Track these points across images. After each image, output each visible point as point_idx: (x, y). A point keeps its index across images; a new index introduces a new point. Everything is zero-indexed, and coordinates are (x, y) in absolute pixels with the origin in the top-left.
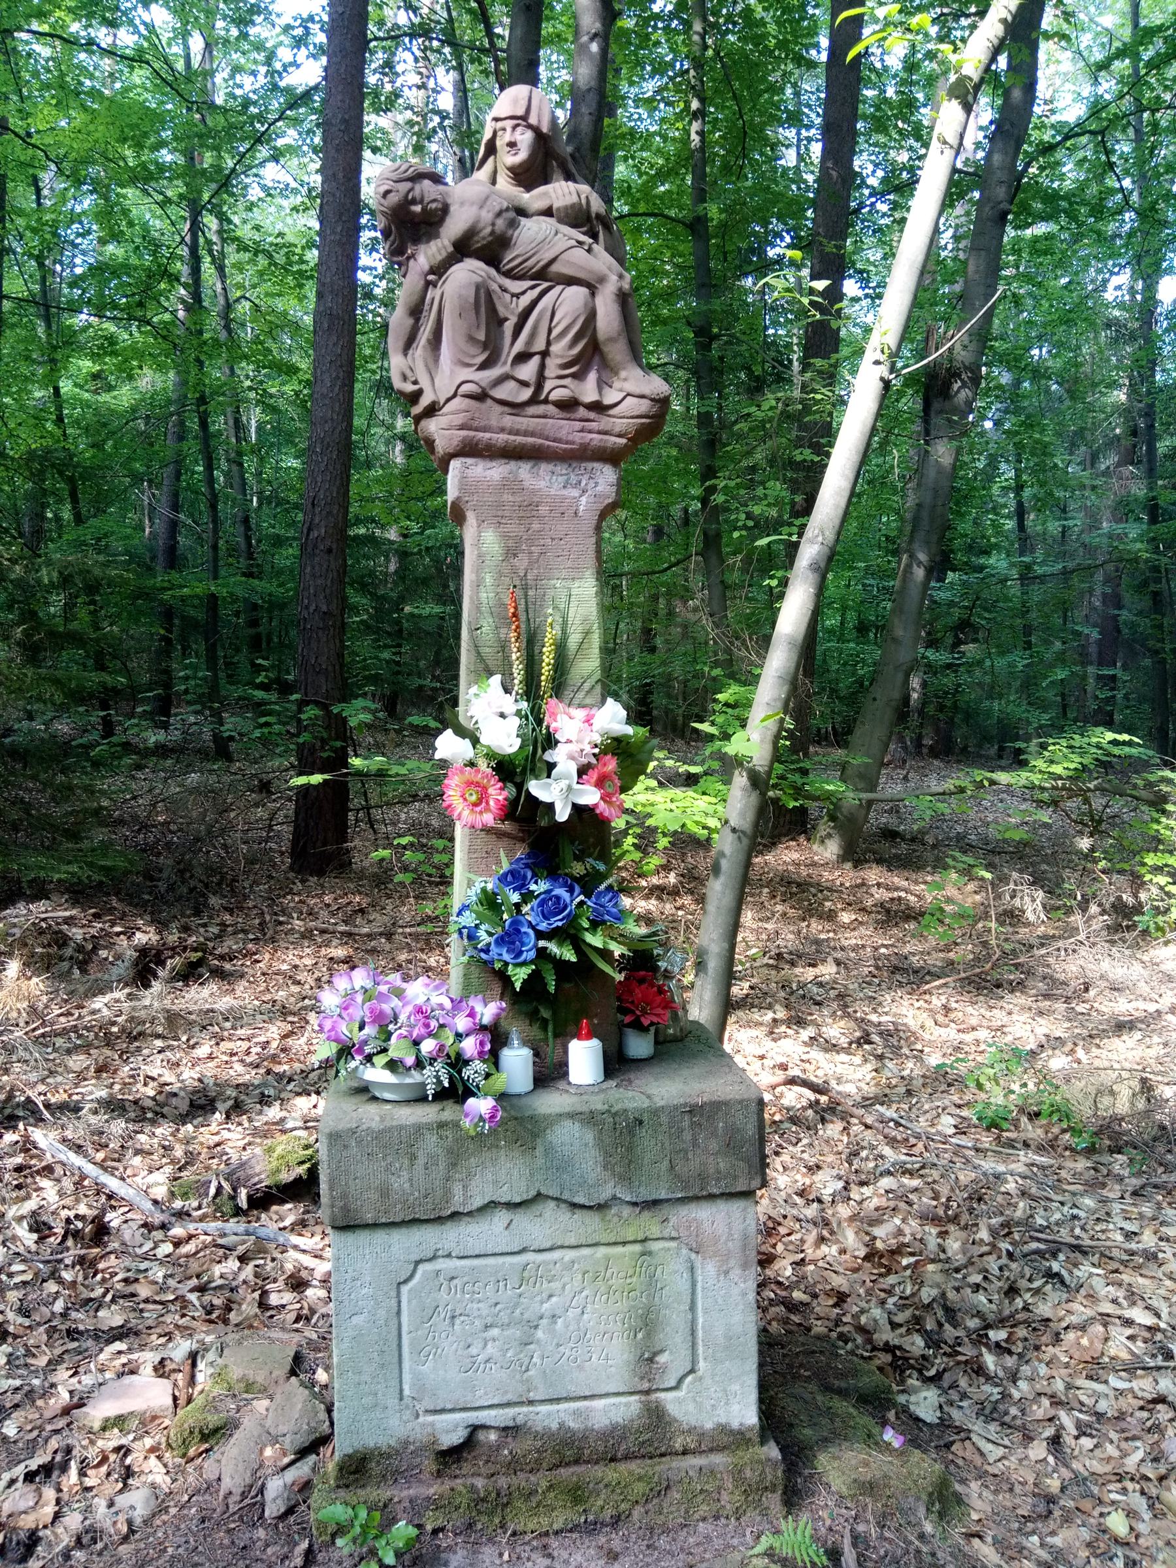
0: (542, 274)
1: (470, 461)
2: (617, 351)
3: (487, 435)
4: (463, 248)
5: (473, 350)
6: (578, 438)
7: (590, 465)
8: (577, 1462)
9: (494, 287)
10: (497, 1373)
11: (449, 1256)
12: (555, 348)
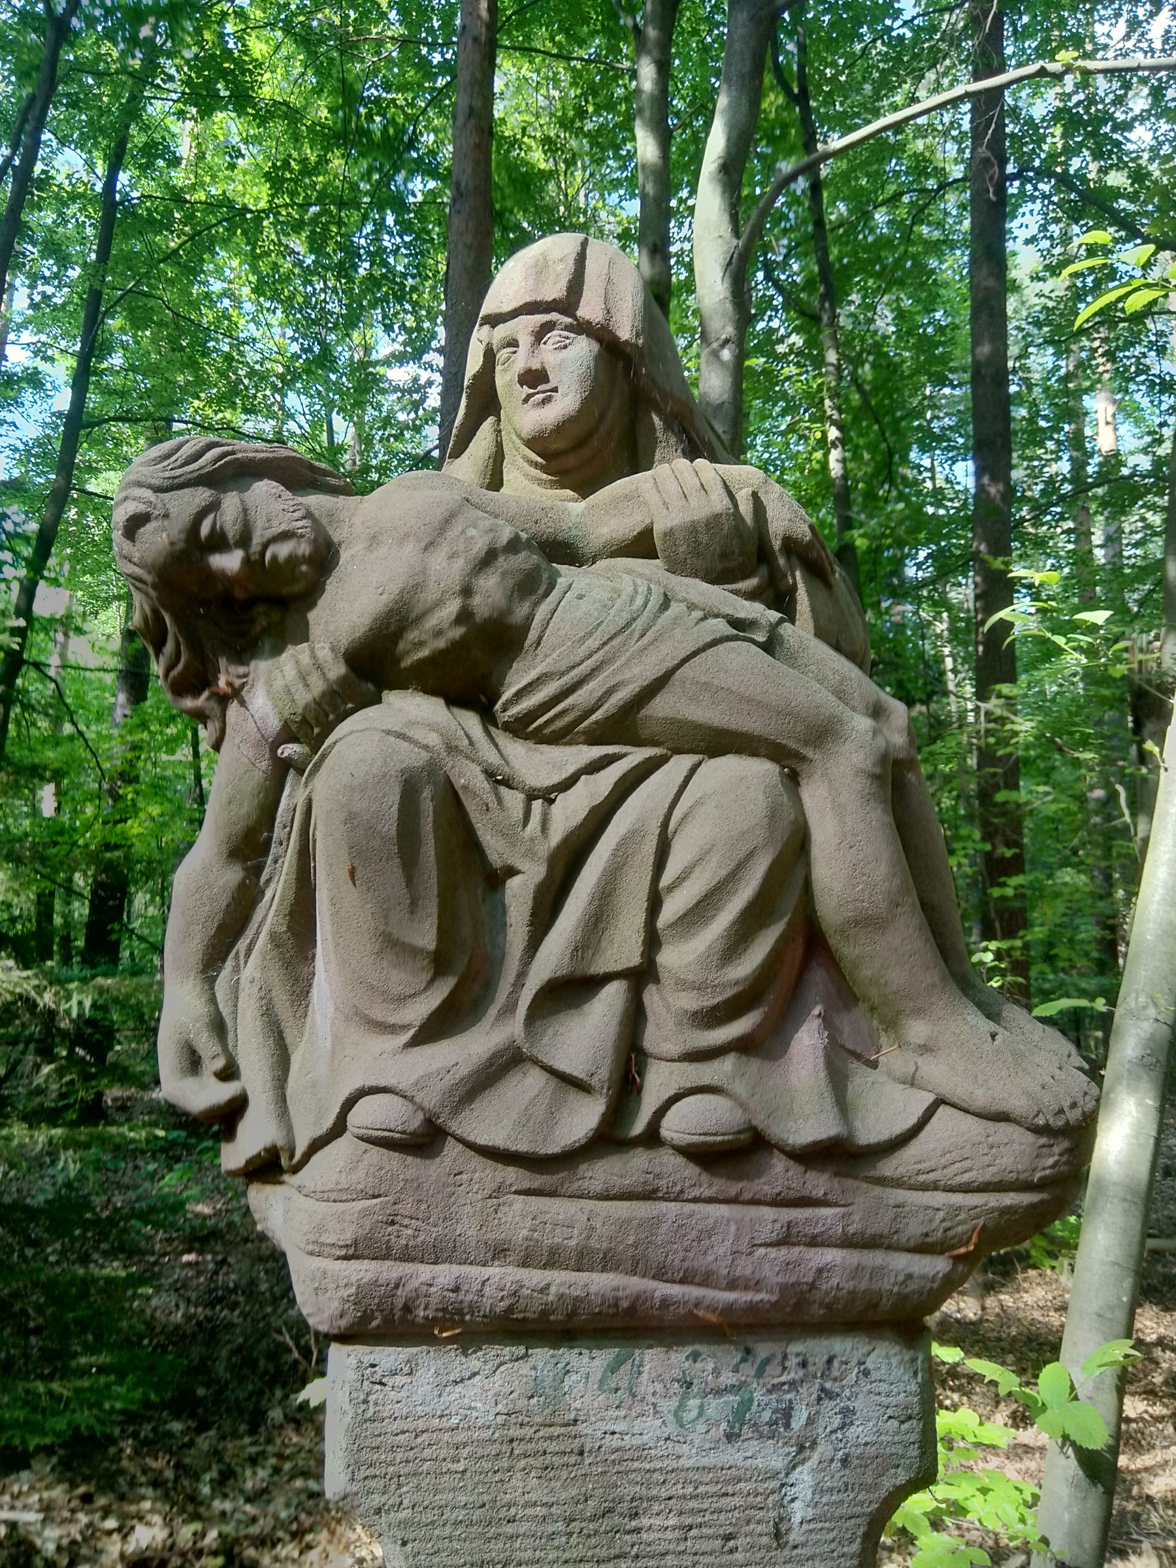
0: (622, 726)
1: (388, 1356)
2: (891, 956)
3: (445, 1274)
4: (373, 667)
5: (399, 979)
6: (772, 1267)
7: (818, 1348)
9: (469, 776)
12: (670, 958)
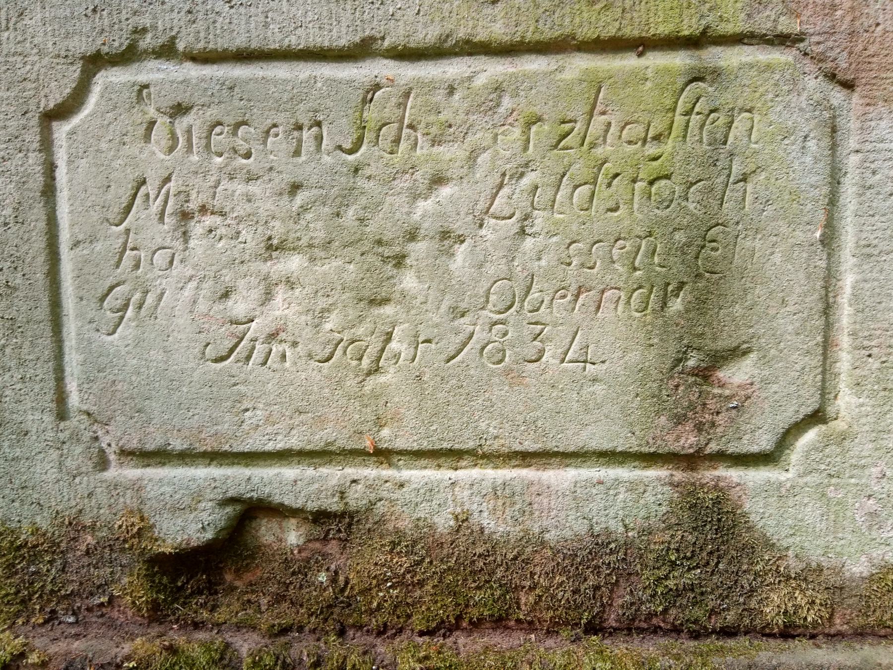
8: (499, 622)
10: (298, 371)
11: (167, 51)
